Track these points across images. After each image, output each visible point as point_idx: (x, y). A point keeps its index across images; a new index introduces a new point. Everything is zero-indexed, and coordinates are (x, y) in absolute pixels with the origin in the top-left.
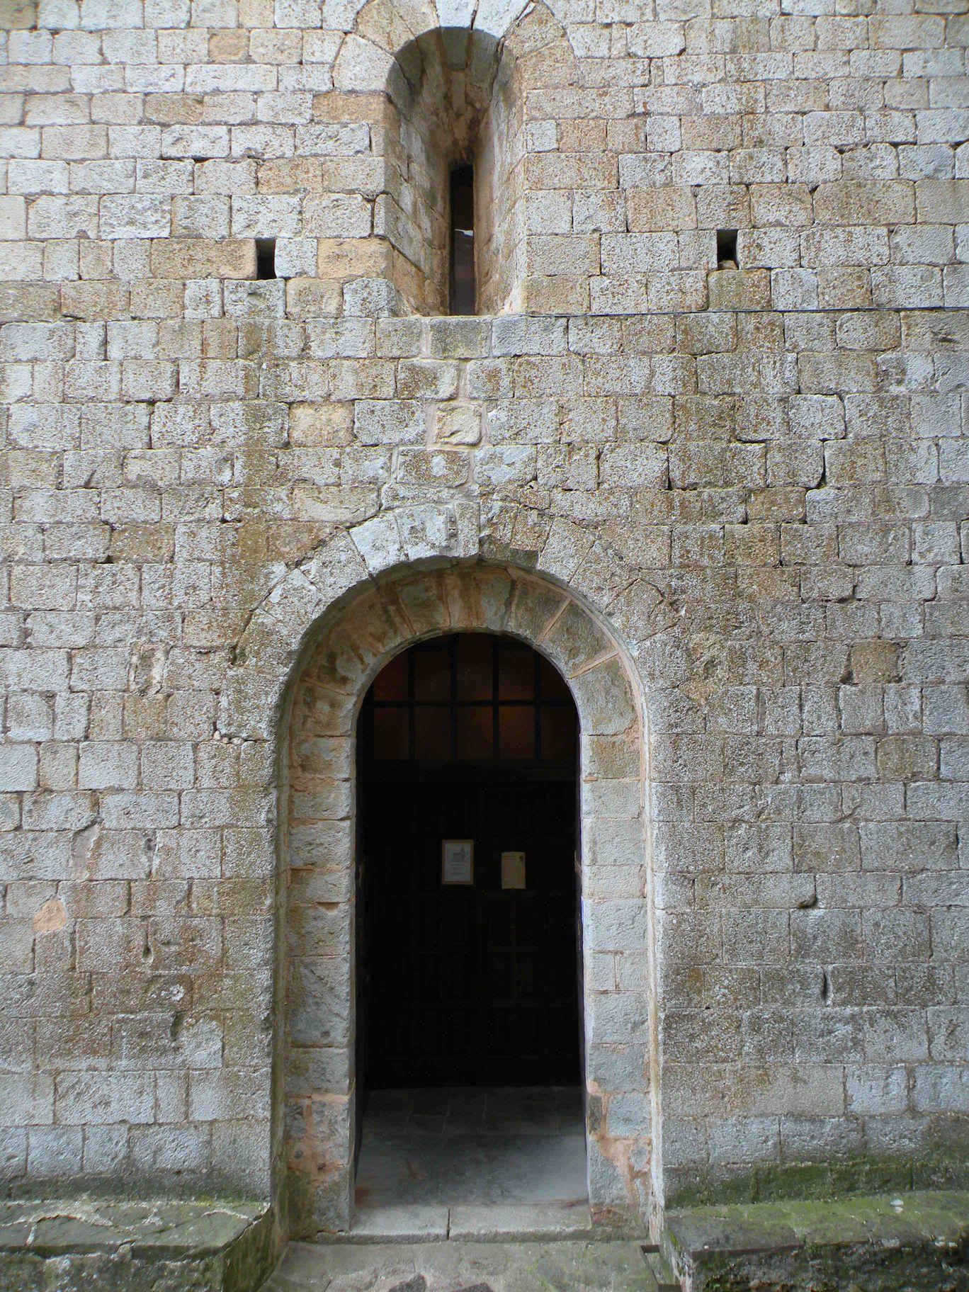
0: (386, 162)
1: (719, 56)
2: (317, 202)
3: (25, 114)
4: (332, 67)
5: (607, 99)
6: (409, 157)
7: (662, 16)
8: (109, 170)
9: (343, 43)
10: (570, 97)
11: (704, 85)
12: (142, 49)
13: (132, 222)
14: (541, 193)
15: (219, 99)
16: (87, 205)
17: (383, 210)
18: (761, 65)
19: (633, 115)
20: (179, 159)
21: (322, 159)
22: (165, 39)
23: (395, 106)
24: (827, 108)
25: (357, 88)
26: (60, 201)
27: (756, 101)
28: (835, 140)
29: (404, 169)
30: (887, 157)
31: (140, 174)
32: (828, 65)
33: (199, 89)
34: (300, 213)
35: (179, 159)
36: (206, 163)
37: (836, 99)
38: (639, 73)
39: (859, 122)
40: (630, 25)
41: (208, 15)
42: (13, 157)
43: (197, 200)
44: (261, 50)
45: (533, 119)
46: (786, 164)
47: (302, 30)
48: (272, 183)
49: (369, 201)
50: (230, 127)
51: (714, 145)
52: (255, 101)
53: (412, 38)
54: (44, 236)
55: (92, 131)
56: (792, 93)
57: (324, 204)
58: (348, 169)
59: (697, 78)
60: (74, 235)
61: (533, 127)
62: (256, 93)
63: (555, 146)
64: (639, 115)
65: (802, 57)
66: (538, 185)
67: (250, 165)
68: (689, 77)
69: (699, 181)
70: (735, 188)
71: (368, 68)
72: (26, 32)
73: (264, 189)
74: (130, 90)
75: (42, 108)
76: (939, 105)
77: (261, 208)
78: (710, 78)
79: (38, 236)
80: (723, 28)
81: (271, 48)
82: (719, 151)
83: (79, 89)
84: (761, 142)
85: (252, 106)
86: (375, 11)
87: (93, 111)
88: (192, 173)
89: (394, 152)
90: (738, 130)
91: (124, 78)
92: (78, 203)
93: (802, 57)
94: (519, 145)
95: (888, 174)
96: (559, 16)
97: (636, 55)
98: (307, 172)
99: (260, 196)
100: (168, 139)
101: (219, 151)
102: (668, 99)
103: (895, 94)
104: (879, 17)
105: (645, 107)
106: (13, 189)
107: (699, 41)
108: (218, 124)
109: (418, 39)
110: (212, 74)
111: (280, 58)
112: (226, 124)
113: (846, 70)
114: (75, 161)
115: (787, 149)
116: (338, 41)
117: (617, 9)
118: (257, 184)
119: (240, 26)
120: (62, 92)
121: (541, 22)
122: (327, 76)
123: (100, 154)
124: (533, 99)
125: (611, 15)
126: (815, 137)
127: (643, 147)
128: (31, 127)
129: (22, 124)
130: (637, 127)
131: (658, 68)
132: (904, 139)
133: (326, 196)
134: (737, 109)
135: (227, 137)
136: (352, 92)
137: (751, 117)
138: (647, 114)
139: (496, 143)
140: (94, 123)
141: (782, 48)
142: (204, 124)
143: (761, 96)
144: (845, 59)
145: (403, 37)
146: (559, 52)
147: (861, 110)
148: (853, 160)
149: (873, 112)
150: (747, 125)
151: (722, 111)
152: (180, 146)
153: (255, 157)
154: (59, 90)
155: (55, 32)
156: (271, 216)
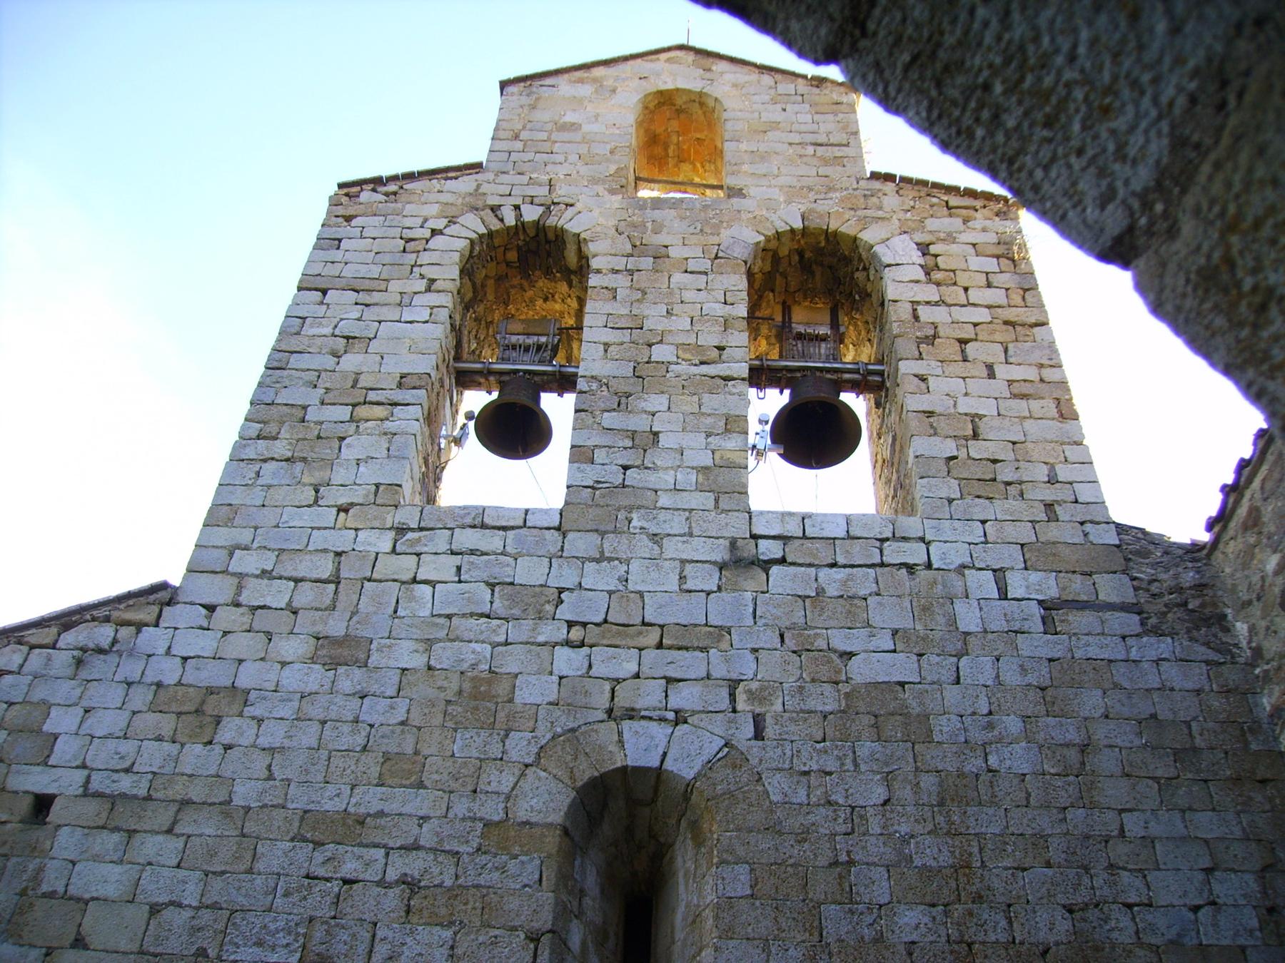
0: (556, 898)
1: (926, 808)
2: (472, 937)
3: (175, 822)
4: (508, 798)
5: (806, 845)
6: (582, 891)
7: (863, 767)
8: (249, 885)
9: (523, 775)
10: (765, 842)
11: (912, 836)
12: (312, 769)
13: (259, 943)
14: (732, 943)
15: (382, 821)
16: (215, 921)
17: (547, 953)
18: (972, 819)
19: (835, 863)
20: (327, 880)
21: (485, 891)
22: (337, 761)
23: (572, 840)
24: (1048, 865)
25: (533, 820)
26: (187, 914)
27: (970, 854)
28: (1061, 899)
29: (575, 904)
30: (1122, 919)
31: (280, 891)
32: (1045, 822)
33: (362, 810)
34: (452, 948)
35: (327, 880)
36: (355, 886)
37: (1055, 854)
38: (841, 821)
39: (1086, 880)
40: (830, 773)
41: (386, 741)
42: (150, 864)
43: (337, 925)
44: (436, 777)
45: (723, 862)
46: (1010, 923)
47: (481, 760)
48: (425, 912)
49: (532, 940)
50: (388, 850)
51: (928, 899)
52: (420, 826)
53: (596, 774)
54: (159, 950)
55: (239, 844)
56: (1009, 849)
57: (481, 939)
58: (513, 903)
59: (904, 829)
60: (192, 952)
61: (726, 871)
62: (422, 818)
63: (749, 892)
64: (842, 864)
65: (1016, 813)
66: (727, 933)
67: (403, 891)
68: (896, 827)
69: (914, 937)
70: (956, 947)
71: (546, 800)
72: (200, 746)
73: (414, 919)
74: (290, 806)
75: (195, 817)
76: (1169, 866)
77: (408, 940)
78: (919, 829)
79: (152, 950)
80: (928, 781)
81: (445, 775)
82: (934, 905)
83: (238, 801)
84: (981, 897)
85: (416, 830)
86: (559, 747)
87: (247, 824)
88: (338, 896)
89: (566, 886)
90: (954, 885)
91: (286, 795)
92: (206, 916)
93: (1016, 813)
94: (708, 888)
95: (1126, 937)
96: (754, 761)
97: (837, 803)
98: (465, 904)
99: (409, 926)
100: (319, 857)
101: (372, 875)
102: (875, 848)
103: (1119, 851)
104: (1090, 778)
105: (849, 855)
106: (140, 898)
107: (906, 793)
108: (376, 846)
109: (603, 776)
110: (379, 796)
111: (454, 785)
112: (385, 846)
113: (1064, 827)
114: (214, 873)
115: (1009, 906)
116: (517, 773)
117: (815, 758)
118: (408, 912)
119: (416, 753)
120: (220, 804)
121: (734, 766)
122: (502, 805)
123: (243, 868)
124: (725, 842)
125: (809, 763)
126: (1039, 895)
127: (848, 897)
128: (178, 836)
129: (170, 831)
130: (840, 876)
131: (861, 817)
132: (1137, 900)
133: (483, 931)
134: (951, 861)
135: (384, 861)
136: (527, 823)
137: (967, 871)
138: (851, 863)
139: (681, 880)
140: (244, 836)
141: (994, 802)
142: (361, 845)
143: (976, 850)
144: (1061, 816)
145: (586, 773)
146: (754, 796)
147: (1087, 869)
148: (1084, 920)
149: (1099, 869)
150: (962, 880)
151: (934, 864)
152: (330, 866)
153: (410, 884)
154: (217, 801)
155: (228, 747)
156: (419, 949)
